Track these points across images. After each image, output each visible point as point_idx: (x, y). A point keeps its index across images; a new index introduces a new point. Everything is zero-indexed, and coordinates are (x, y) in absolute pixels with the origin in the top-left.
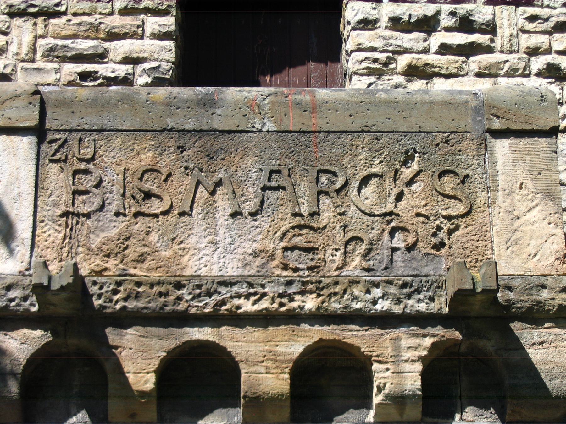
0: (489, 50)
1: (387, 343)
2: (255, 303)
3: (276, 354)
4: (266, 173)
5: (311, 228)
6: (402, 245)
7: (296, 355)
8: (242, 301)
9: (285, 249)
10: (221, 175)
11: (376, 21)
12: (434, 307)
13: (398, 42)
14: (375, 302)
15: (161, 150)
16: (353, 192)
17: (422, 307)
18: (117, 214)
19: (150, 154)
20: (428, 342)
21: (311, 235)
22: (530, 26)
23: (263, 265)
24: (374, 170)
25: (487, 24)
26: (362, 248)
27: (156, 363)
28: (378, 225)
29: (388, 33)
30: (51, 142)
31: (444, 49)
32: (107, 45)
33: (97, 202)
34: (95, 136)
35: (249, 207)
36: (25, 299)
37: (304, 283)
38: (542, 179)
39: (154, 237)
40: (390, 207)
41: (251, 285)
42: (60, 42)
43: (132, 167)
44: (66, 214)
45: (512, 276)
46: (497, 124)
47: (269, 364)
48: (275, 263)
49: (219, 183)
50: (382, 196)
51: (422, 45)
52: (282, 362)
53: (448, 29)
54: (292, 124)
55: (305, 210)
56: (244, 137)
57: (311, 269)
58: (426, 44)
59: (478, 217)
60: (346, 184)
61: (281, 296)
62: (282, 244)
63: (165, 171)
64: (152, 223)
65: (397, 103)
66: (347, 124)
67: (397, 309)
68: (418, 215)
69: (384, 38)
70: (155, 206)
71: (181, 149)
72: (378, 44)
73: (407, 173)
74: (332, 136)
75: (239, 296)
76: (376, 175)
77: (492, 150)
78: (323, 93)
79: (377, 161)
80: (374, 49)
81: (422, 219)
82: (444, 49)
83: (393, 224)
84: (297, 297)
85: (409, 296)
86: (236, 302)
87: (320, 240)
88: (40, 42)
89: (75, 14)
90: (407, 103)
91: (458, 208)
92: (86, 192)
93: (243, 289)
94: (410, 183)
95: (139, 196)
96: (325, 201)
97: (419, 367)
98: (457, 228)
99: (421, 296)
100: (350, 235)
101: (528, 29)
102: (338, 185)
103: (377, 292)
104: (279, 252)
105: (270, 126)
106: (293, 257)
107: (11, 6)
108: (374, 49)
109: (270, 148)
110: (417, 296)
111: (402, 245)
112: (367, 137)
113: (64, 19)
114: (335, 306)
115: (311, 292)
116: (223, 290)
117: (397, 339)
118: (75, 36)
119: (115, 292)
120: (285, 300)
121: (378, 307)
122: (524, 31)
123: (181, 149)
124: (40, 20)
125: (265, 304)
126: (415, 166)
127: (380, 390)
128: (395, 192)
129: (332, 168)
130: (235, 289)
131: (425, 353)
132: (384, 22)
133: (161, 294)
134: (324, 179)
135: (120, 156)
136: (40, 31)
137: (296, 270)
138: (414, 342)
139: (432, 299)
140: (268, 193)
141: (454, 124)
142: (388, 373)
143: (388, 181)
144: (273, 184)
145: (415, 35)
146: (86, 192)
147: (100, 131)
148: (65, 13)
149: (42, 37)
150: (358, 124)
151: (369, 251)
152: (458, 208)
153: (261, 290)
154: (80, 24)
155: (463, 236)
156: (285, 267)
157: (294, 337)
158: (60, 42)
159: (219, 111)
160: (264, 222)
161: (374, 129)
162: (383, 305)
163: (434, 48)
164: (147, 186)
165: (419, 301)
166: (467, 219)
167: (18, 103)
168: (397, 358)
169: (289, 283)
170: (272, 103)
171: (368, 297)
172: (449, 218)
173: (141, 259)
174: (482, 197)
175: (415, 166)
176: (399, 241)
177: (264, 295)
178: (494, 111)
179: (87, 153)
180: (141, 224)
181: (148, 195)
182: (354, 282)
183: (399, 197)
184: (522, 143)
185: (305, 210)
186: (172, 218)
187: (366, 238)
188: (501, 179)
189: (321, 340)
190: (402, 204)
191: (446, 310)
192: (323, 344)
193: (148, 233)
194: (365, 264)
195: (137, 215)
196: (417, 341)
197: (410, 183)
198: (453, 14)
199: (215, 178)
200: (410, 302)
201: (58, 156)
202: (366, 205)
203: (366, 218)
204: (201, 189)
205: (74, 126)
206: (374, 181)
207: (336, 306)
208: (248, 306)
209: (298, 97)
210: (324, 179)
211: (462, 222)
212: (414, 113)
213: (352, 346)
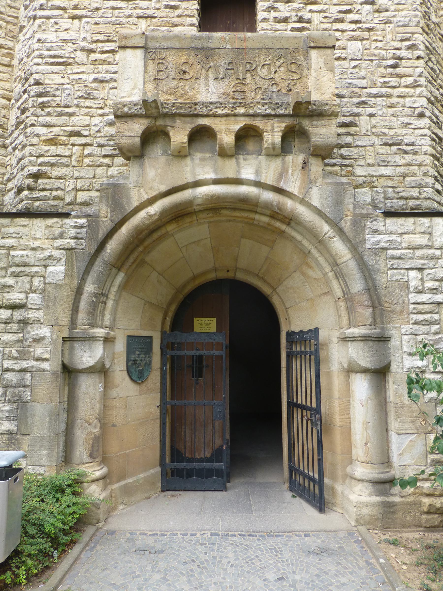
0: (308, 29)
1: (269, 125)
2: (222, 110)
3: (230, 129)
4: (227, 63)
5: (243, 84)
6: (275, 90)
7: (237, 130)
8: (218, 110)
9: (234, 91)
10: (211, 64)
11: (268, 19)
12: (287, 112)
13: (276, 27)
14: (265, 110)
15: (189, 55)
16: (259, 70)
17: (282, 112)
18: (173, 79)
19: (185, 57)
20: (284, 125)
21: (243, 87)
22: (324, 21)
23: (226, 98)
24: (267, 63)
25: (309, 19)
26: (261, 92)
27: (188, 132)
28: (268, 83)
29: (273, 23)
30: (150, 52)
31: (293, 29)
32: (172, 29)
33: (166, 75)
34: (165, 50)
35: (220, 76)
36: (141, 109)
37: (240, 103)
38: (328, 65)
39: (187, 88)
40: (272, 76)
41: (221, 104)
42: (155, 28)
43: (179, 62)
44: (155, 79)
45: (316, 101)
46: (312, 45)
47: (227, 133)
48: (230, 97)
49: (210, 67)
50: (269, 72)
51: (285, 28)
52: (232, 132)
53: (294, 22)
54: (237, 45)
55: (241, 77)
56: (219, 50)
57: (243, 99)
58: (286, 27)
59: (305, 80)
60: (256, 67)
61: (233, 108)
62: (232, 90)
63: (191, 63)
64: (186, 82)
65: (276, 37)
66: (258, 45)
67: (273, 113)
68: (282, 79)
69: (271, 25)
70: (187, 76)
71: (197, 55)
72: (269, 27)
73: (278, 64)
74: (252, 50)
75: (216, 108)
76: (267, 64)
77: (310, 55)
78: (249, 34)
79: (268, 59)
80: (267, 29)
81: (283, 80)
82: (293, 29)
83: (273, 82)
84: (238, 108)
85: (278, 108)
86: (216, 110)
87: (246, 89)
88: (149, 28)
89: (161, 17)
90: (279, 37)
91: (296, 77)
92: (162, 71)
93: (219, 105)
94: (280, 67)
95: (181, 73)
96: (248, 75)
97: (280, 134)
98: (296, 84)
99: (282, 108)
100: (257, 86)
101: (291, 191)
102: (253, 68)
103: (266, 107)
104: (232, 93)
105: (229, 46)
106: (237, 95)
107: (138, 14)
108: (267, 29)
109: (229, 55)
110: (280, 108)
111: (275, 90)
112: (264, 50)
113: (157, 19)
114: (251, 112)
115: (243, 106)
116: (211, 106)
117: (273, 124)
118: (160, 26)
119: (173, 106)
120: (233, 109)
121: (267, 112)
122: (322, 22)
123: (197, 55)
124: (148, 19)
125: (226, 111)
126: (281, 61)
127: (266, 142)
128: (274, 70)
129: (251, 62)
130: (216, 105)
131: (283, 129)
132: (271, 20)
133: (189, 107)
134: (248, 66)
135: (175, 58)
136: (148, 24)
137: (237, 99)
138: (279, 125)
139: (286, 109)
140: (228, 71)
141: (297, 45)
142: (270, 136)
143: (272, 67)
144: (230, 68)
145: (282, 24)
146: (162, 71)
147: (167, 48)
148: (156, 17)
149: (149, 26)
150: (261, 45)
151: (263, 93)
152: (296, 77)
153: (225, 106)
154: (162, 21)
155: (298, 87)
156: (233, 98)
157: (237, 122)
158: (155, 28)
159: (211, 41)
160: (226, 82)
161: (267, 47)
162: (269, 111)
163: (289, 29)
164: (184, 69)
165: (282, 110)
166: (300, 81)
167: (137, 37)
168: (273, 131)
169: (235, 103)
170: (230, 38)
171: (263, 108)
172: (293, 80)
173: (182, 96)
174: (305, 72)
175: (281, 61)
176: (275, 89)
177: (226, 107)
178: (312, 40)
179: (162, 56)
180: (182, 83)
181: (184, 72)
182: (258, 103)
183: (275, 72)
184: (322, 52)
185: (241, 77)
186: (193, 81)
187: (263, 87)
188: (313, 65)
189: (246, 124)
190: (277, 75)
191: (291, 113)
192: (246, 126)
193: (185, 86)
194: (262, 97)
195: (180, 79)
196: (280, 125)
197: (280, 67)
198: (296, 15)
199: (209, 66)
200: (278, 110)
201: (151, 58)
202: (263, 75)
203: (263, 80)
204: (203, 70)
205: (158, 46)
206: (266, 66)
207: (251, 111)
208: (220, 112)
209: (240, 36)
210: (248, 66)
211: (298, 82)
212: (282, 41)
213: (256, 126)
